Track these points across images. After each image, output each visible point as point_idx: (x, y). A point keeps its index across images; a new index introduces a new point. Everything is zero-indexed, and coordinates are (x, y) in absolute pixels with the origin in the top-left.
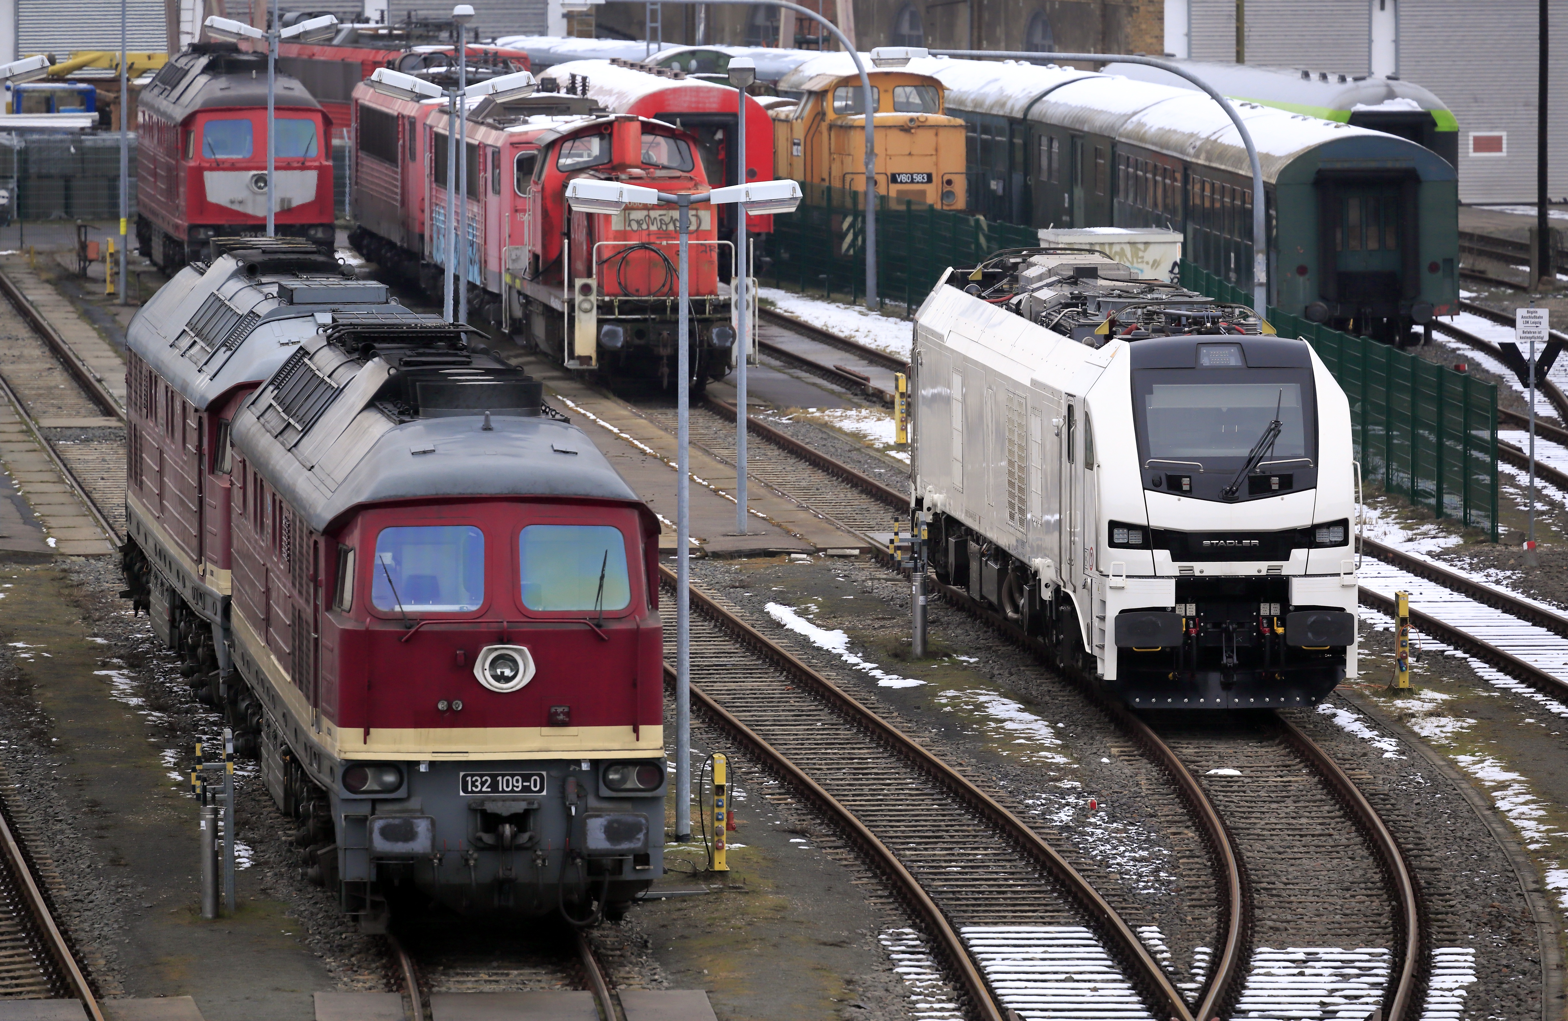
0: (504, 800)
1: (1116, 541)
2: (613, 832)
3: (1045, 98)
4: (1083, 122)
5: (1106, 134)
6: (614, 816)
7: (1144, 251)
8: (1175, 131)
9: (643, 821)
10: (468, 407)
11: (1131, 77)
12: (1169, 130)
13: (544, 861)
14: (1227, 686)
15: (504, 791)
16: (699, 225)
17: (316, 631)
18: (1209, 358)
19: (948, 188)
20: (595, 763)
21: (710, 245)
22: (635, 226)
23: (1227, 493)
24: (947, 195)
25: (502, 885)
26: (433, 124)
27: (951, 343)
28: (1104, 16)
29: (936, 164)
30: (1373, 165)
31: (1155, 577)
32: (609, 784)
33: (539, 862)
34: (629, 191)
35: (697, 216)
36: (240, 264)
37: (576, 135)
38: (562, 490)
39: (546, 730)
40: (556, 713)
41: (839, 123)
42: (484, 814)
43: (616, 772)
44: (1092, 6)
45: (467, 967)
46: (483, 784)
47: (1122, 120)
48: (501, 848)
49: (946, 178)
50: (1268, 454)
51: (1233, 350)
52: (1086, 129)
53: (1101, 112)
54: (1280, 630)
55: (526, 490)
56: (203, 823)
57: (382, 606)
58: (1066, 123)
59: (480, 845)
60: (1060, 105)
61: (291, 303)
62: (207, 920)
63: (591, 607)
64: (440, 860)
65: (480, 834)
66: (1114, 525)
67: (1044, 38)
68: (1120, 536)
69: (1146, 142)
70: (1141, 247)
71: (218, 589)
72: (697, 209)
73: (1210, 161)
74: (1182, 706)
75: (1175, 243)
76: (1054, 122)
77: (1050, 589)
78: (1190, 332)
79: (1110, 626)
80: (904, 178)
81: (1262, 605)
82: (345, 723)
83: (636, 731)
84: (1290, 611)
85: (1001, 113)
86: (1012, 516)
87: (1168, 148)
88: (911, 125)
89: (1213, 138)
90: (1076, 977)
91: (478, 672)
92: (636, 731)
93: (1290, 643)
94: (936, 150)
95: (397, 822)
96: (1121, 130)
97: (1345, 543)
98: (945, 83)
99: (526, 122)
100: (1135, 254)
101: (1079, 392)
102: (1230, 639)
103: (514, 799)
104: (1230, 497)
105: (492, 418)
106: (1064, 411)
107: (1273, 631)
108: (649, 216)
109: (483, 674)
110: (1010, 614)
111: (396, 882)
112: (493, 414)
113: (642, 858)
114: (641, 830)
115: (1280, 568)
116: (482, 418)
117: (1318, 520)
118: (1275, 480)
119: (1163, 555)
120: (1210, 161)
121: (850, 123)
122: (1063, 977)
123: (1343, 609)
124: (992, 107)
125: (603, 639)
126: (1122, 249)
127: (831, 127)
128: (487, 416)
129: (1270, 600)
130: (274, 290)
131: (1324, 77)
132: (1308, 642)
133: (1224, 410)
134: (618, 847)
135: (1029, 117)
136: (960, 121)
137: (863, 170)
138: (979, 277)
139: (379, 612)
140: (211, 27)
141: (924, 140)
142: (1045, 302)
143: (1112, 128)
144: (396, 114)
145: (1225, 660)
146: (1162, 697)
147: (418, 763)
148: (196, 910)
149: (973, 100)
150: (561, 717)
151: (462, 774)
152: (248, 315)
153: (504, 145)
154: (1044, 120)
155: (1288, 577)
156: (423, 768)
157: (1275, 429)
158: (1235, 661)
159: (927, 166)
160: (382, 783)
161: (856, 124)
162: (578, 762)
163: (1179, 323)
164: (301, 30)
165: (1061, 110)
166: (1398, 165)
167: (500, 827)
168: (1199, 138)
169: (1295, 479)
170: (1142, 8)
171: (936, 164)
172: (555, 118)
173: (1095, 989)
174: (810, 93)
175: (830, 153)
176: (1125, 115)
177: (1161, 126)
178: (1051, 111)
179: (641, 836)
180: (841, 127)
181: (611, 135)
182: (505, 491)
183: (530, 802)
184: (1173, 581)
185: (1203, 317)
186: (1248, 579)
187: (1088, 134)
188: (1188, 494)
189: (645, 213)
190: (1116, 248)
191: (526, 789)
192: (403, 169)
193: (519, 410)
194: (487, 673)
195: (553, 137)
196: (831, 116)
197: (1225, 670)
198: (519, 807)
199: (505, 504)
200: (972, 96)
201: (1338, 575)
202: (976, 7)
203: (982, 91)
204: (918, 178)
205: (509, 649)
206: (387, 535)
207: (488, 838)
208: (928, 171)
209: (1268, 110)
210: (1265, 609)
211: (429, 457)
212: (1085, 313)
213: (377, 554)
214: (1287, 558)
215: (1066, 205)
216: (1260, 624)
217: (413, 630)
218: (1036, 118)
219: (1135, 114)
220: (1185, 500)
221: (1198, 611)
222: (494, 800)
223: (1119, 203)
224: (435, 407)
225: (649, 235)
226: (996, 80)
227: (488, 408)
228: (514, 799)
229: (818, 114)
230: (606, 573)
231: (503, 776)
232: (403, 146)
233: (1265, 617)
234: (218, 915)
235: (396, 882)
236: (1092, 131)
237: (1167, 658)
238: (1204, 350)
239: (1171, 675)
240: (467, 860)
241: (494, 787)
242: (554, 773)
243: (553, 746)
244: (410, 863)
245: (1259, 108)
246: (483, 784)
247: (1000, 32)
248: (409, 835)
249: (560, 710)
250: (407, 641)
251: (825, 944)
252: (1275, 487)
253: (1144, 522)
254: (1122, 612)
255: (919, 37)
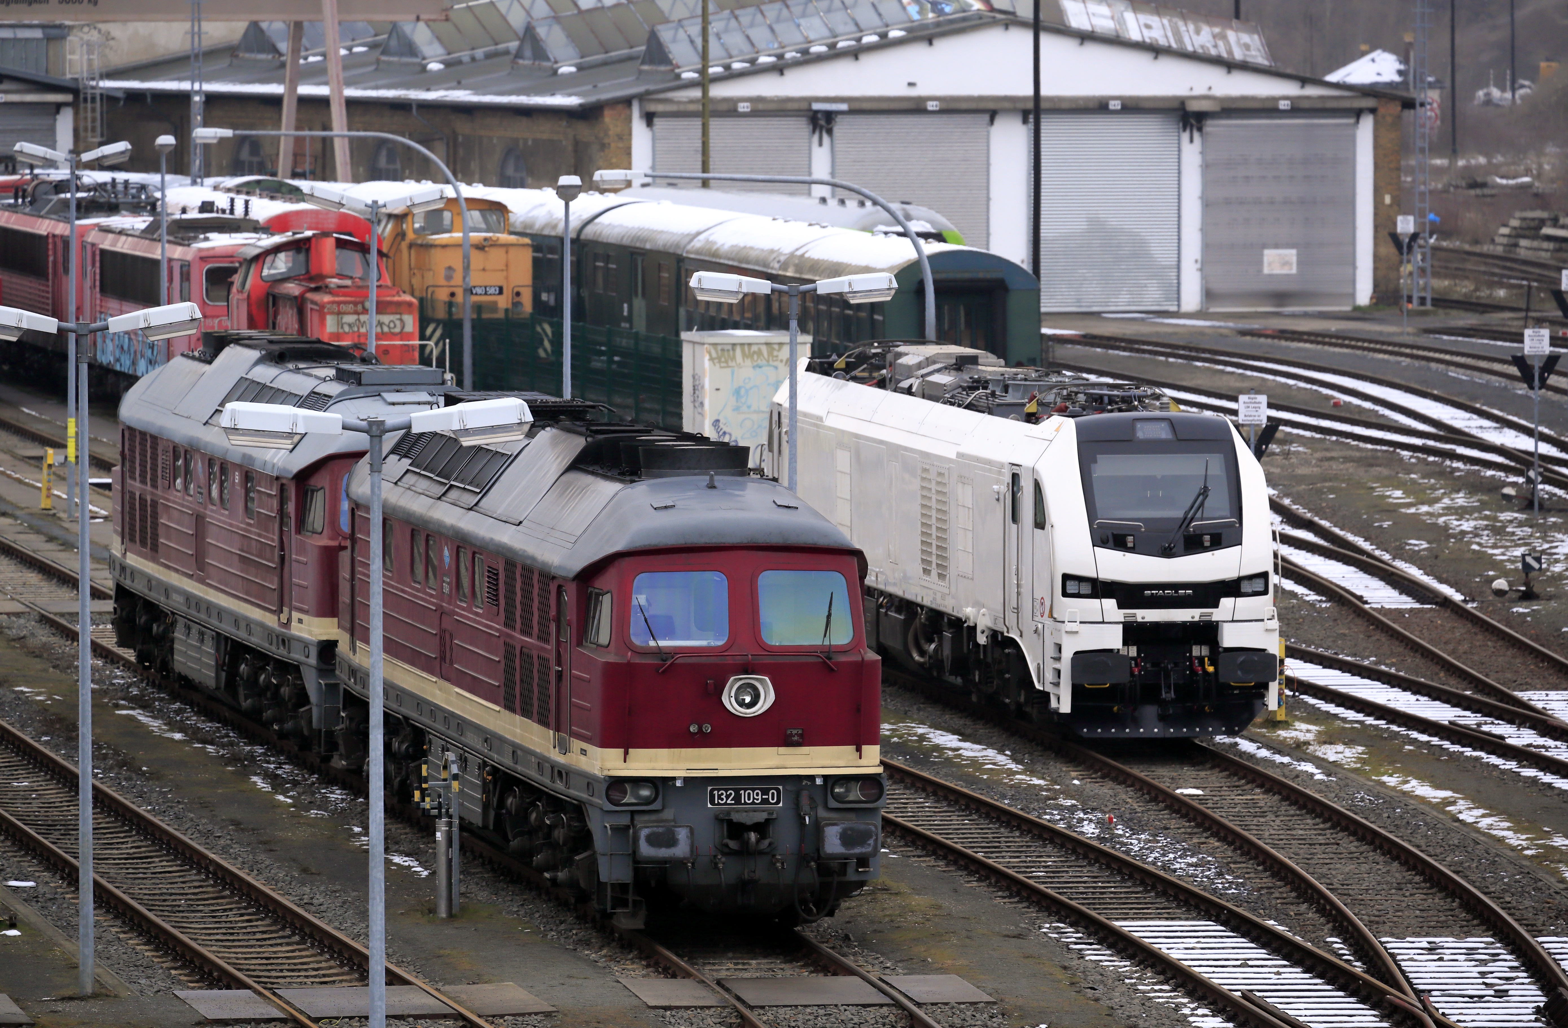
0: (746, 811)
1: (1069, 591)
2: (847, 839)
3: (597, 220)
4: (645, 240)
5: (671, 251)
6: (847, 824)
7: (779, 350)
8: (752, 248)
9: (873, 829)
10: (689, 468)
11: (676, 201)
12: (745, 247)
13: (783, 864)
14: (1163, 718)
15: (745, 803)
16: (403, 327)
17: (559, 664)
18: (1144, 432)
19: (516, 299)
20: (825, 777)
21: (413, 346)
22: (347, 329)
23: (1165, 549)
24: (516, 304)
25: (745, 885)
26: (96, 241)
27: (831, 422)
28: (576, 151)
29: (507, 278)
30: (967, 276)
31: (1103, 622)
32: (838, 798)
33: (779, 865)
34: (747, 282)
35: (401, 320)
36: (263, 352)
37: (277, 249)
38: (793, 540)
39: (782, 750)
40: (791, 735)
41: (419, 242)
42: (730, 823)
43: (841, 787)
44: (564, 143)
45: (715, 959)
46: (728, 797)
47: (687, 239)
48: (745, 852)
49: (516, 290)
50: (1199, 515)
51: (1164, 425)
52: (648, 246)
53: (662, 232)
54: (1211, 669)
55: (762, 540)
56: (438, 834)
57: (637, 641)
58: (626, 242)
59: (727, 850)
60: (615, 227)
61: (359, 384)
62: (443, 919)
63: (819, 642)
64: (693, 864)
65: (727, 841)
66: (1066, 577)
67: (516, 169)
68: (1072, 587)
69: (720, 258)
70: (776, 347)
71: (311, 635)
72: (400, 314)
73: (801, 273)
74: (1110, 736)
75: (805, 343)
76: (611, 240)
77: (985, 634)
78: (1111, 411)
79: (1065, 665)
80: (479, 290)
81: (1194, 647)
82: (606, 743)
83: (859, 750)
84: (1219, 653)
85: (553, 233)
86: (926, 572)
87: (748, 263)
88: (485, 244)
89: (799, 253)
90: (1250, 963)
91: (725, 699)
92: (859, 750)
93: (1222, 680)
94: (507, 266)
95: (660, 830)
96: (689, 247)
97: (1265, 592)
98: (510, 207)
99: (207, 239)
100: (770, 354)
101: (1026, 461)
102: (1167, 676)
103: (755, 810)
104: (1167, 553)
105: (716, 478)
106: (1008, 479)
107: (1204, 669)
108: (359, 320)
109: (729, 701)
110: (917, 657)
111: (653, 883)
112: (716, 474)
113: (863, 861)
114: (871, 837)
115: (1211, 614)
116: (708, 478)
117: (1244, 573)
118: (1207, 538)
119: (1110, 604)
120: (801, 273)
121: (431, 242)
122: (1239, 963)
123: (1264, 650)
124: (543, 228)
125: (832, 670)
126: (760, 350)
127: (411, 246)
128: (712, 476)
129: (1200, 643)
130: (332, 372)
131: (842, 202)
132: (1236, 678)
133: (1159, 477)
134: (852, 852)
135: (582, 237)
136: (527, 241)
137: (443, 282)
138: (843, 366)
139: (636, 646)
140: (21, 152)
141: (496, 257)
142: (945, 385)
143: (677, 245)
144: (45, 233)
145: (1164, 696)
146: (1106, 727)
147: (674, 779)
148: (432, 910)
149: (522, 223)
150: (796, 738)
151: (709, 788)
152: (309, 395)
153: (194, 259)
154: (600, 240)
155: (1217, 622)
156: (679, 784)
157: (1204, 492)
158: (1173, 696)
159: (497, 279)
160: (638, 797)
161: (437, 243)
162: (812, 778)
163: (1102, 402)
164: (100, 155)
165: (616, 231)
166: (989, 276)
167: (746, 835)
168: (781, 254)
169: (1224, 537)
170: (613, 145)
171: (507, 278)
172: (233, 235)
173: (1278, 973)
174: (390, 216)
175: (410, 269)
176: (688, 235)
177: (734, 242)
178: (606, 232)
179: (871, 842)
180: (421, 246)
181: (308, 251)
182: (745, 541)
183: (770, 813)
184: (1121, 626)
185: (1130, 397)
186: (1184, 624)
187: (651, 251)
188: (1132, 550)
189: (355, 317)
190: (754, 348)
191: (765, 802)
192: (53, 282)
193: (732, 471)
194: (733, 700)
195: (257, 251)
196: (411, 236)
197: (1162, 703)
198: (761, 817)
199: (745, 552)
200: (521, 219)
201: (1262, 620)
202: (451, 144)
203: (531, 215)
204: (491, 291)
205: (753, 679)
206: (642, 579)
207: (733, 844)
208: (500, 284)
209: (836, 230)
210: (1196, 651)
211: (670, 511)
212: (993, 394)
213: (634, 596)
214: (1216, 606)
215: (625, 313)
216: (1192, 664)
217: (669, 662)
218: (590, 237)
219: (699, 234)
220: (1129, 555)
221: (1139, 652)
222: (738, 811)
223: (688, 312)
224: (659, 468)
225: (359, 336)
226: (542, 205)
227: (712, 468)
228: (755, 810)
229: (397, 235)
230: (833, 612)
231: (745, 790)
232: (55, 262)
233: (1197, 658)
234: (451, 916)
235: (653, 883)
236: (655, 248)
237: (1114, 693)
238: (1139, 425)
239: (1115, 708)
240: (716, 864)
241: (737, 799)
242: (788, 787)
243: (788, 764)
244: (664, 867)
245: (829, 228)
246: (728, 797)
247: (474, 165)
248: (672, 842)
249: (794, 732)
250: (663, 672)
251: (1008, 936)
252: (1207, 544)
253: (1093, 575)
254: (1076, 653)
255: (395, 171)
